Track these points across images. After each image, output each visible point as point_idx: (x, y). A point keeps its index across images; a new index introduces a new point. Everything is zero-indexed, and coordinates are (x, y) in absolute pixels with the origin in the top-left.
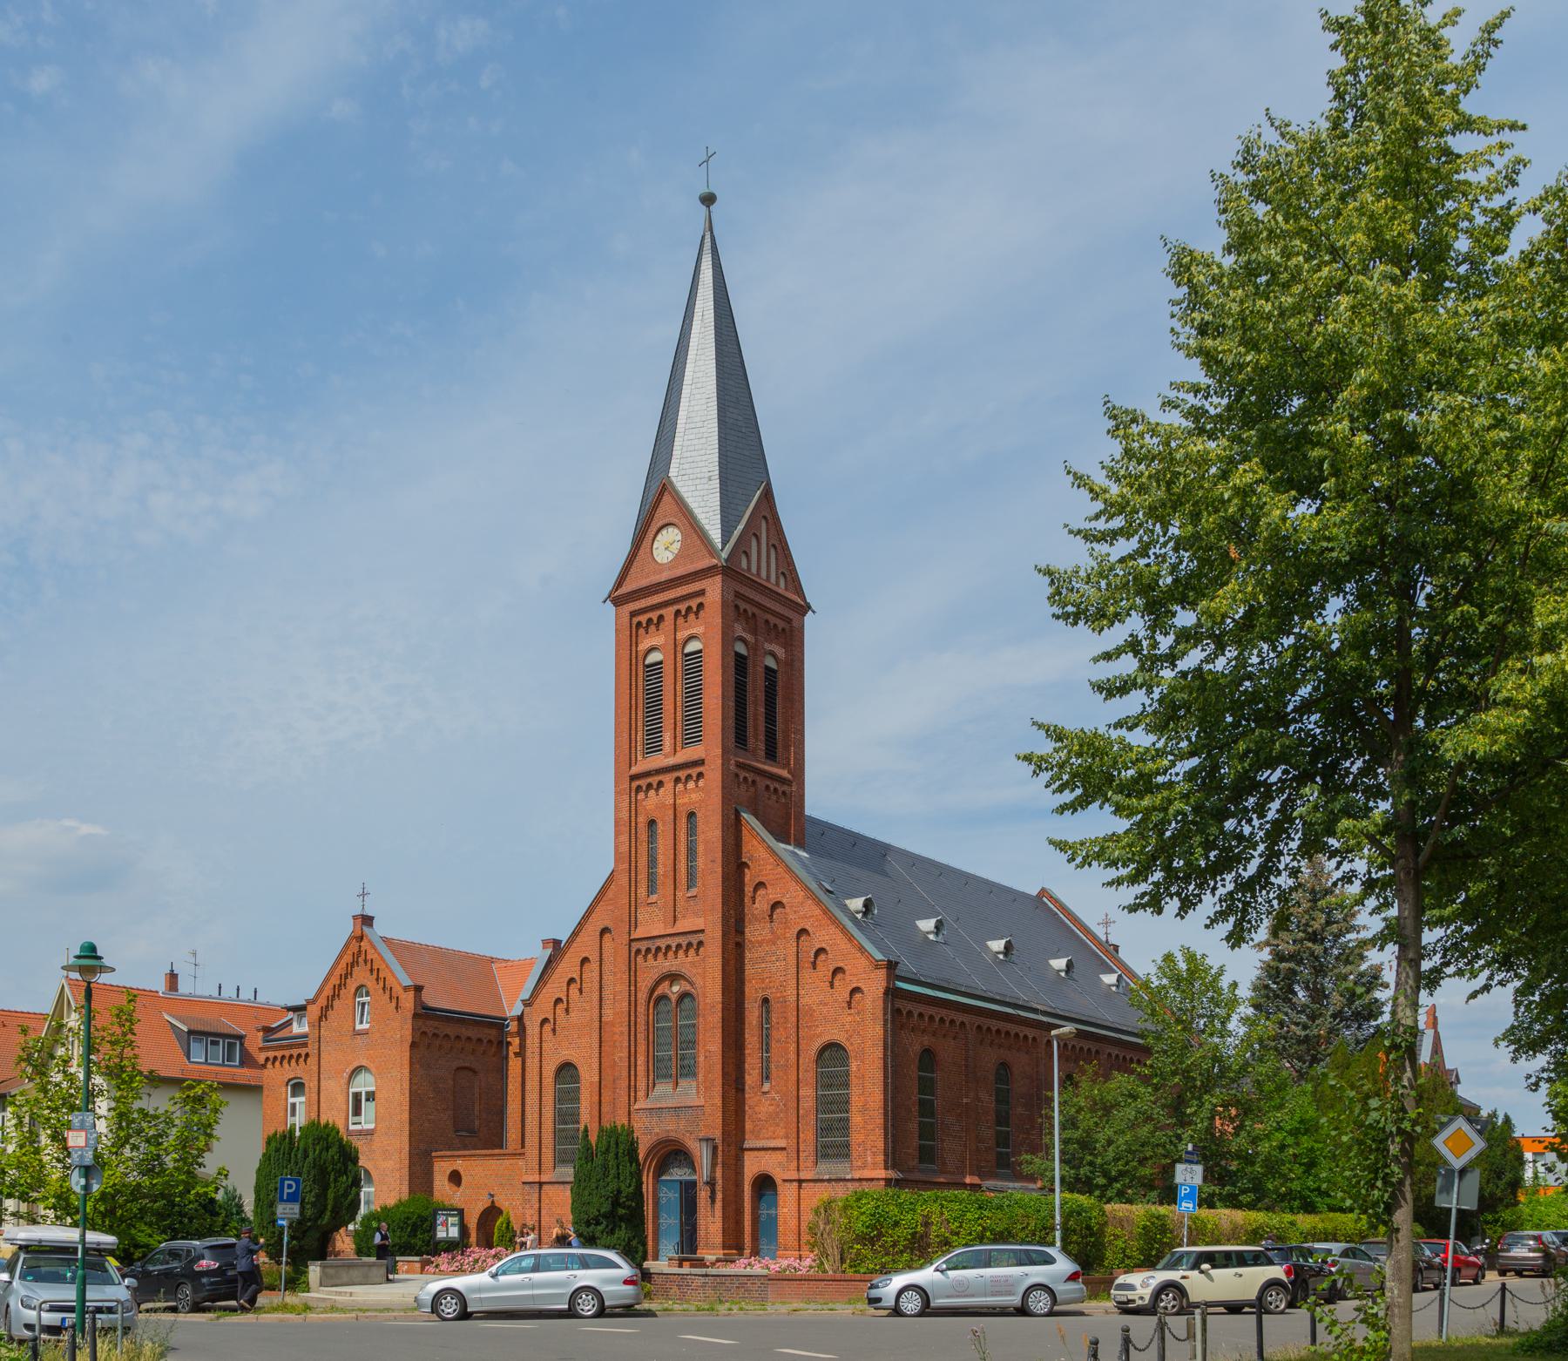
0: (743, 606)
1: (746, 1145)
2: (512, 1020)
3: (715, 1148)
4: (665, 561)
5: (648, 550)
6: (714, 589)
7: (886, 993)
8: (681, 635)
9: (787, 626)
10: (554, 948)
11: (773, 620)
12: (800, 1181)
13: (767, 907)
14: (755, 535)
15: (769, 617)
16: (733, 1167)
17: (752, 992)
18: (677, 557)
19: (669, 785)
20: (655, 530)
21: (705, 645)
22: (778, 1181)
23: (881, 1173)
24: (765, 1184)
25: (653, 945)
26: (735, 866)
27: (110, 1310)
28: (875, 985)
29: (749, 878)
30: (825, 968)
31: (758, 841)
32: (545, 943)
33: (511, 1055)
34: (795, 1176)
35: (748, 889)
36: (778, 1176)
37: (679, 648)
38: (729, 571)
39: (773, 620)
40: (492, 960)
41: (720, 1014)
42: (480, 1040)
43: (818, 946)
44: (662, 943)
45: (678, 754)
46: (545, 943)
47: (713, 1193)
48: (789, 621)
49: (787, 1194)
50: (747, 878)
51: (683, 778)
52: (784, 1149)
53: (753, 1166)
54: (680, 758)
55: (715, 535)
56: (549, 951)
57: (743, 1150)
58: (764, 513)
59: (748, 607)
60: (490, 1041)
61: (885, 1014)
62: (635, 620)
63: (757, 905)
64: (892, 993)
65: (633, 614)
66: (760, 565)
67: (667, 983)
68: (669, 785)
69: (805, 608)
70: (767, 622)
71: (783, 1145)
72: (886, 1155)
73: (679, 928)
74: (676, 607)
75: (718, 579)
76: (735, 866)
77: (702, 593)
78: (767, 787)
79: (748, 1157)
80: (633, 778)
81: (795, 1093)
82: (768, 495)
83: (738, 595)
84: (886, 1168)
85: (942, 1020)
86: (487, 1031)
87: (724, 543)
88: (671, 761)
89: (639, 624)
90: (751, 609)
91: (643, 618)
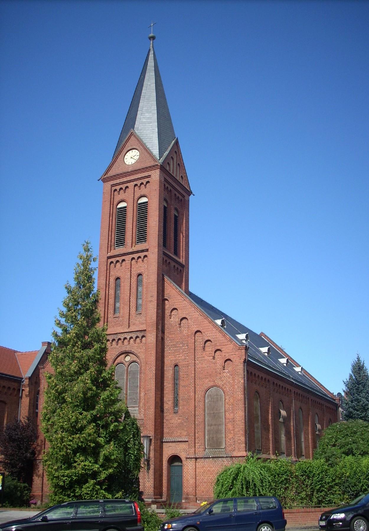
0: (167, 185)
1: (164, 441)
2: (26, 379)
3: (151, 440)
4: (130, 164)
5: (122, 159)
6: (156, 175)
7: (245, 362)
8: (137, 195)
9: (183, 199)
10: (48, 346)
11: (178, 195)
12: (196, 459)
13: (178, 320)
14: (172, 157)
15: (176, 193)
16: (159, 452)
17: (169, 361)
18: (137, 162)
19: (128, 262)
20: (125, 152)
21: (149, 201)
22: (183, 459)
23: (244, 453)
24: (175, 459)
25: (116, 337)
26: (162, 300)
27: (216, 341)
28: (238, 358)
29: (168, 306)
30: (210, 348)
31: (171, 288)
32: (44, 344)
33: (24, 396)
34: (195, 457)
35: (167, 312)
36: (183, 456)
37: (136, 200)
38: (162, 168)
39: (178, 195)
40: (15, 352)
41: (154, 372)
42: (9, 388)
43: (207, 339)
44: (122, 337)
45: (133, 248)
46: (44, 344)
47: (148, 465)
48: (184, 196)
49: (188, 467)
50: (167, 307)
51: (136, 258)
52: (187, 441)
53: (168, 451)
54: (135, 249)
55: (156, 152)
56: (45, 347)
57: (162, 442)
58: (175, 150)
59: (169, 186)
60: (14, 389)
61: (244, 372)
62: (114, 188)
63: (172, 319)
64: (247, 363)
65: (113, 186)
66: (172, 169)
67: (123, 356)
68: (128, 262)
69: (189, 193)
70: (175, 195)
71: (186, 440)
72: (246, 444)
73: (132, 328)
74: (135, 183)
75: (158, 171)
76: (162, 300)
77: (149, 176)
78: (174, 266)
79: (165, 445)
80: (109, 258)
81: (193, 412)
82: (177, 143)
83: (166, 180)
84: (246, 451)
85: (265, 379)
86: (13, 384)
87: (160, 157)
88: (131, 250)
89: (115, 190)
90: (170, 188)
91: (118, 188)
